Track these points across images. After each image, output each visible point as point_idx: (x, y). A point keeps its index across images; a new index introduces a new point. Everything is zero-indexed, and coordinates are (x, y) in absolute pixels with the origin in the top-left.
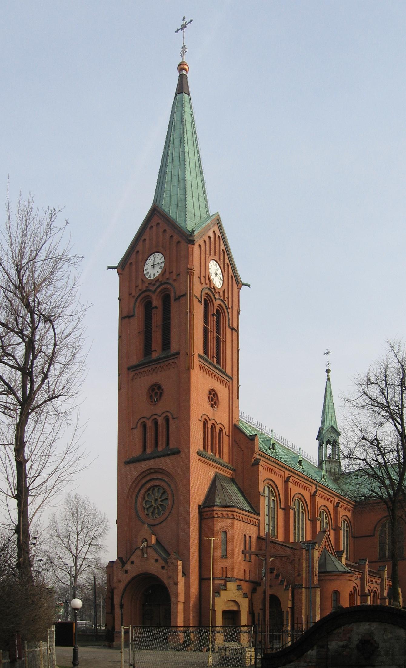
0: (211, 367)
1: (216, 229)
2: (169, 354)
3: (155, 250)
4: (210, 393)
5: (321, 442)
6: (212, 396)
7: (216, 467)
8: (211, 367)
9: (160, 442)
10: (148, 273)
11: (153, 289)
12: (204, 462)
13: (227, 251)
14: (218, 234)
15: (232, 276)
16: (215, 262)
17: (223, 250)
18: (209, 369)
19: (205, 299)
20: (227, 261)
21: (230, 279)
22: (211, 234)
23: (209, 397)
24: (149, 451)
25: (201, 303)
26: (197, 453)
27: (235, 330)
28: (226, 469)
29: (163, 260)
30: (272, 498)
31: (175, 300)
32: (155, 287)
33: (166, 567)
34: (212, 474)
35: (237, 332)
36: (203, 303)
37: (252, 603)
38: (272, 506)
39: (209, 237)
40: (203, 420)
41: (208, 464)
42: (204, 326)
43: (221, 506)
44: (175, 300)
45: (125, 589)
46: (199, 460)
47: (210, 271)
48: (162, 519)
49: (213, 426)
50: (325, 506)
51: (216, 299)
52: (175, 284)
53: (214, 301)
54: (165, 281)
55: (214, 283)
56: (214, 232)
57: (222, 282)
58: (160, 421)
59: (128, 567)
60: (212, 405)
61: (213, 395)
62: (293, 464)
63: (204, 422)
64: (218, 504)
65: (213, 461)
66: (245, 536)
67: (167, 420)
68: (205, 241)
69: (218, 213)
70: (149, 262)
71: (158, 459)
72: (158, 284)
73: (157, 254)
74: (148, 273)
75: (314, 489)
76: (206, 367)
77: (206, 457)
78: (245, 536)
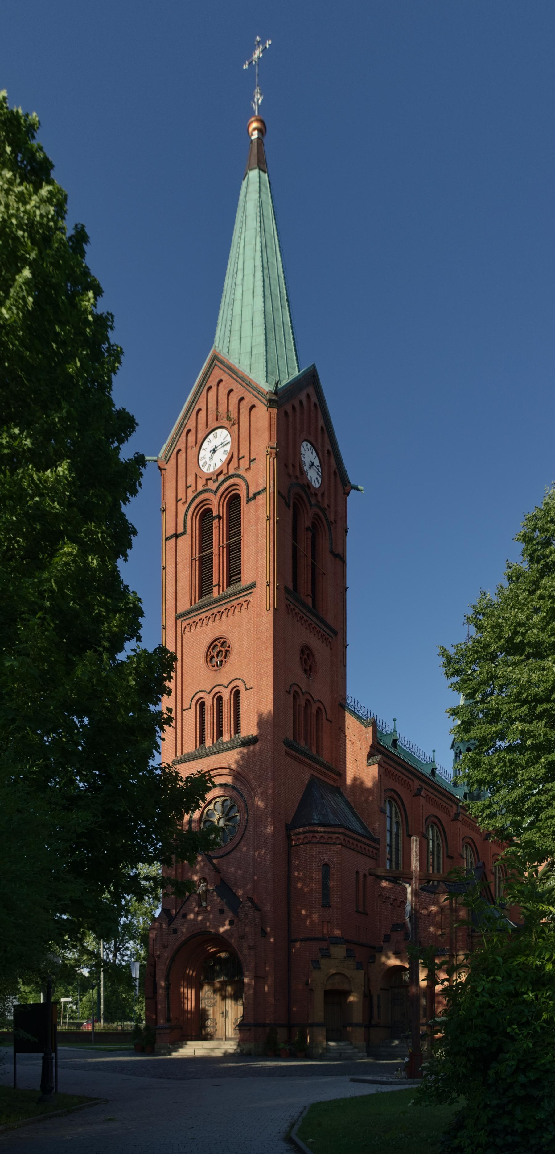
0: (304, 611)
1: (311, 390)
2: (241, 588)
3: (216, 424)
4: (302, 651)
5: (458, 751)
6: (305, 656)
7: (312, 767)
8: (304, 611)
9: (225, 728)
10: (206, 463)
11: (212, 486)
12: (295, 758)
13: (328, 429)
14: (314, 399)
15: (335, 473)
16: (309, 445)
17: (322, 428)
18: (301, 614)
19: (294, 503)
20: (328, 447)
21: (332, 476)
22: (303, 397)
23: (301, 658)
24: (208, 743)
25: (289, 506)
26: (284, 743)
27: (340, 558)
28: (327, 772)
29: (229, 439)
30: (394, 820)
31: (249, 500)
32: (217, 484)
33: (236, 921)
34: (306, 778)
35: (344, 562)
36: (291, 508)
37: (369, 979)
38: (395, 830)
39: (301, 402)
40: (292, 693)
41: (301, 762)
42: (293, 544)
43: (320, 825)
44: (249, 500)
45: (173, 959)
46: (287, 754)
47: (303, 459)
48: (229, 848)
49: (308, 703)
50: (470, 838)
51: (311, 505)
52: (247, 476)
53: (308, 507)
54: (232, 472)
55: (309, 477)
56: (308, 396)
57: (320, 480)
58: (226, 694)
59: (177, 923)
60: (305, 671)
61: (308, 655)
62: (428, 772)
63: (294, 696)
64: (317, 822)
65: (310, 757)
66: (357, 872)
67: (237, 694)
68: (294, 408)
69: (314, 365)
70: (207, 446)
71: (225, 753)
72: (221, 478)
73: (219, 431)
74: (206, 463)
75: (455, 811)
76: (297, 610)
77: (297, 750)
78: (357, 872)
